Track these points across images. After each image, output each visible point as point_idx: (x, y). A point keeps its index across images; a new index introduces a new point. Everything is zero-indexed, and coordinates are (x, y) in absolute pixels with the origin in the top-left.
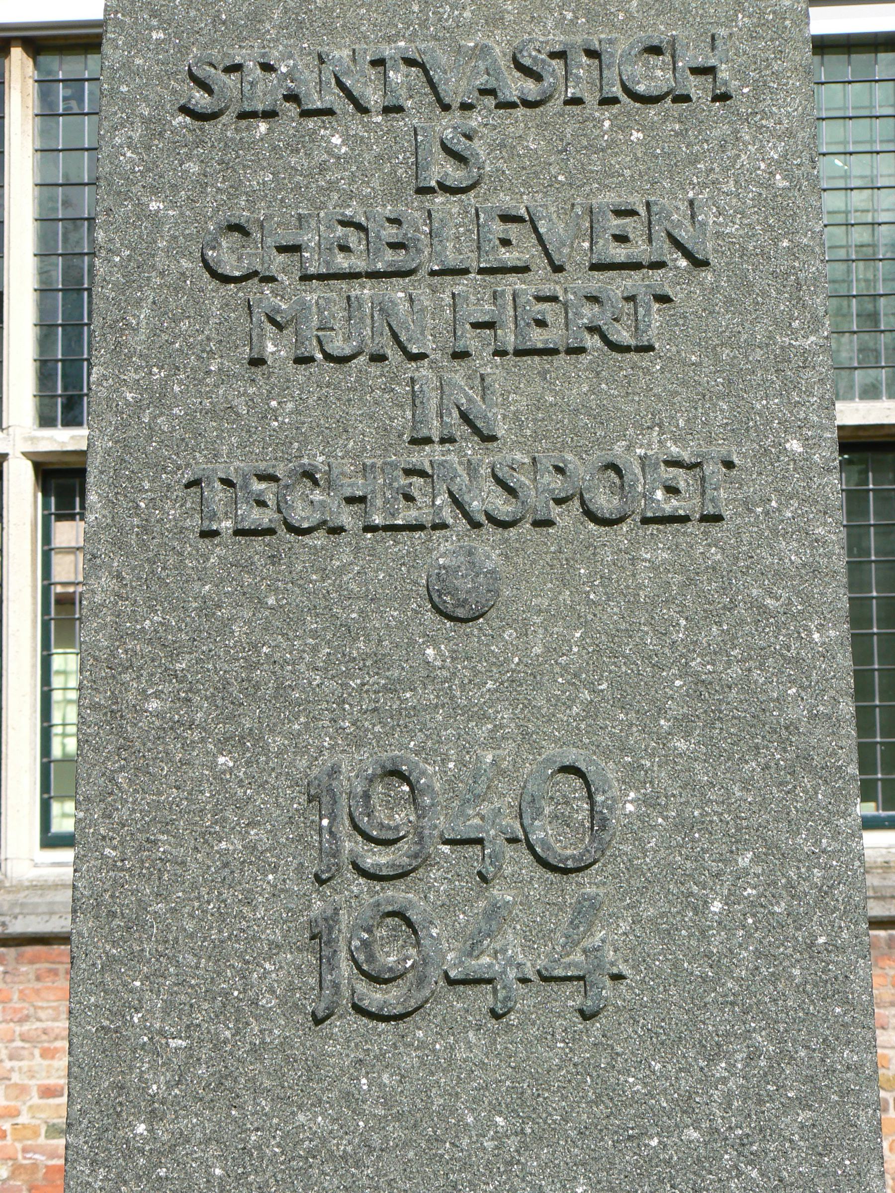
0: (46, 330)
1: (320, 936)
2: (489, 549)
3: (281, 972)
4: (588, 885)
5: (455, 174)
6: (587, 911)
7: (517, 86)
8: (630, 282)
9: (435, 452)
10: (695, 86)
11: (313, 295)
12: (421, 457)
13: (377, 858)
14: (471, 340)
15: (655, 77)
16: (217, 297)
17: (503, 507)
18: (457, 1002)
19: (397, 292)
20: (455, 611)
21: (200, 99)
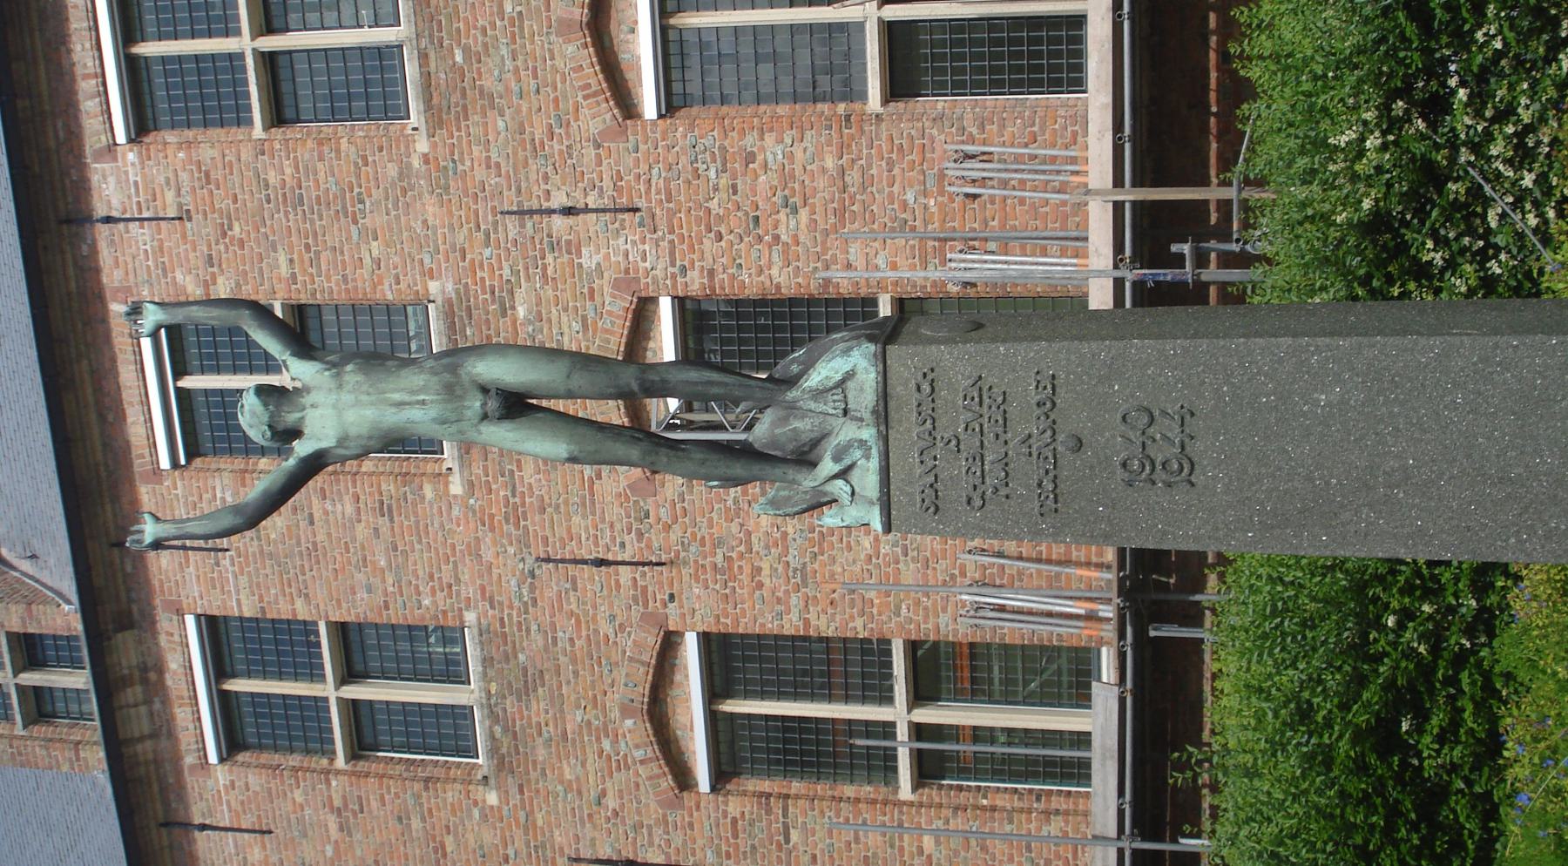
0: (867, 723)
1: (1169, 485)
2: (1061, 437)
3: (1180, 495)
4: (1156, 413)
5: (954, 442)
6: (1164, 413)
7: (928, 424)
8: (985, 397)
9: (1034, 450)
10: (929, 377)
11: (987, 480)
12: (1035, 455)
13: (1186, 470)
14: (1002, 439)
15: (926, 387)
16: (988, 507)
17: (1049, 433)
18: (1188, 449)
19: (988, 459)
20: (1079, 444)
21: (932, 509)
